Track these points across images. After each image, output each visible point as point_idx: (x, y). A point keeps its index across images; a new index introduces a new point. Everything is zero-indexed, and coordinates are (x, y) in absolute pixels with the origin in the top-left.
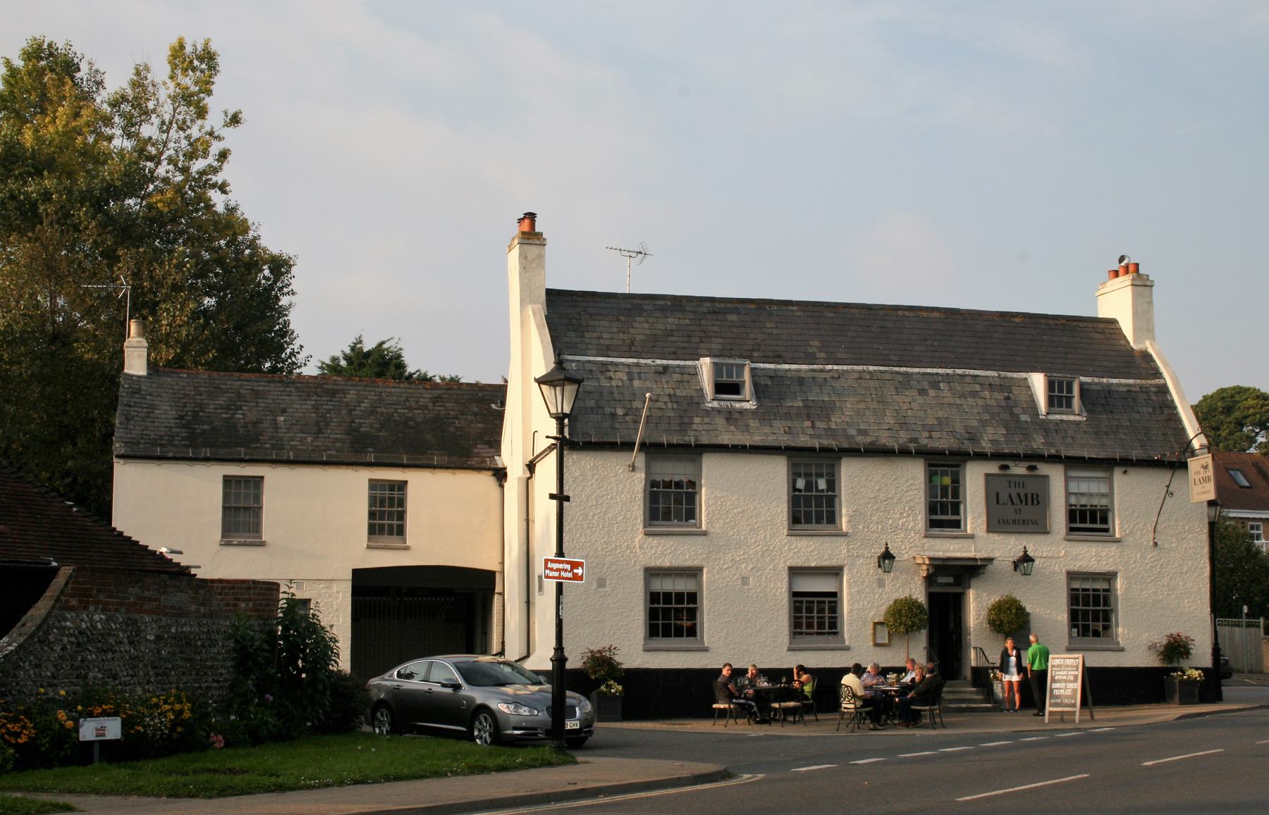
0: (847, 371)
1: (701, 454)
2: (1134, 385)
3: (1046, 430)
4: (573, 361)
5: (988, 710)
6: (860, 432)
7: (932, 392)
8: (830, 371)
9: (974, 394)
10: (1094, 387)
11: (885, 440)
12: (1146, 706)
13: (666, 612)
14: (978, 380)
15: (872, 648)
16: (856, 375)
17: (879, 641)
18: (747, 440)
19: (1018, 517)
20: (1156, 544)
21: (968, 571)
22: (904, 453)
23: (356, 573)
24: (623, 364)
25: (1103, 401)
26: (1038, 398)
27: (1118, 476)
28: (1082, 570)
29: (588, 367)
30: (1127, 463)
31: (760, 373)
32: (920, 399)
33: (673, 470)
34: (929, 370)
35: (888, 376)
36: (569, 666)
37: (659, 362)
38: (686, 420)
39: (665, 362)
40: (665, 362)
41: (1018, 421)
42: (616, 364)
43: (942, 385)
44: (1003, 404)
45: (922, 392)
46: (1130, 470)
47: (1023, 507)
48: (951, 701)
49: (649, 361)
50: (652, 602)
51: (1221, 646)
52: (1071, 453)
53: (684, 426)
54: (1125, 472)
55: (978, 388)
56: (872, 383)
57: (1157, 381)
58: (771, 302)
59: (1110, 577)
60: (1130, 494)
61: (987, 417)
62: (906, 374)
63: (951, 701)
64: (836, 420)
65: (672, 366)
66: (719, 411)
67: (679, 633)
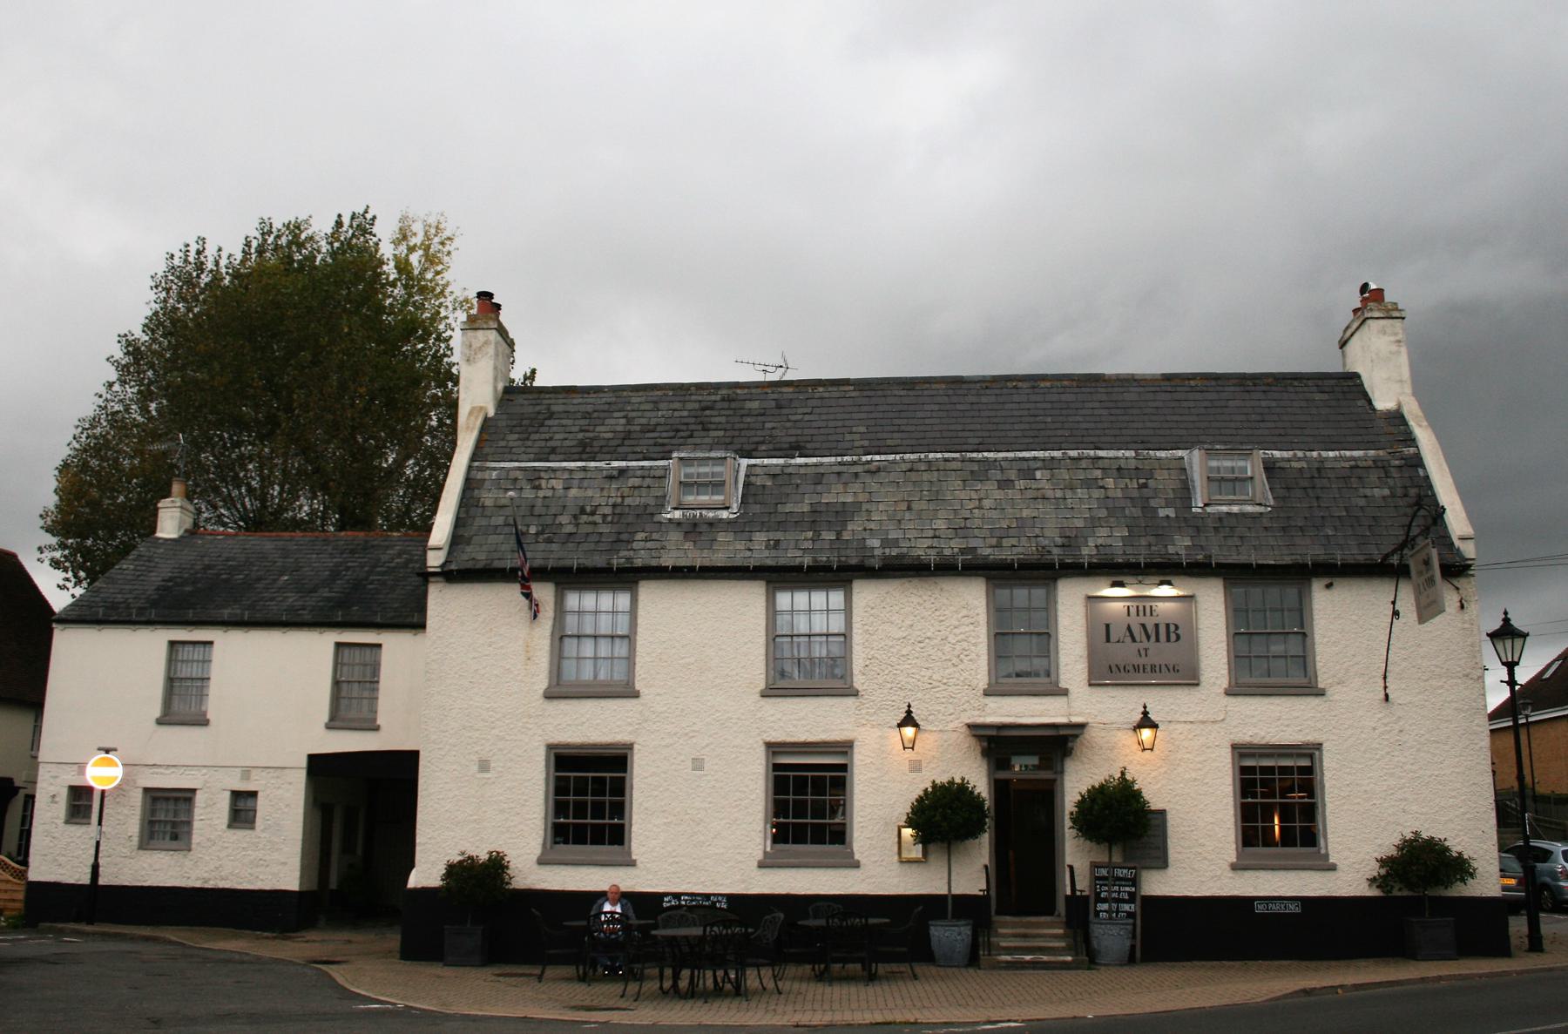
0: (894, 462)
1: (636, 583)
2: (1365, 459)
3: (1198, 529)
4: (494, 469)
5: (1065, 966)
6: (886, 543)
7: (1021, 484)
8: (868, 462)
9: (1089, 484)
10: (1295, 464)
11: (922, 549)
12: (1362, 963)
13: (598, 811)
14: (1101, 464)
15: (897, 865)
16: (904, 467)
17: (905, 855)
18: (719, 558)
19: (1141, 661)
20: (1387, 697)
21: (1058, 743)
22: (945, 569)
23: (313, 759)
24: (565, 469)
25: (1305, 484)
26: (1289, 486)
27: (866, 594)
28: (1256, 741)
29: (513, 475)
30: (1333, 571)
31: (758, 471)
32: (998, 494)
33: (813, 609)
34: (1040, 454)
35: (954, 465)
36: (101, 882)
37: (616, 464)
38: (624, 537)
39: (623, 464)
40: (623, 464)
41: (1155, 516)
42: (554, 470)
43: (1038, 474)
44: (1135, 494)
45: (1005, 484)
46: (1337, 581)
47: (1152, 644)
48: (1009, 950)
49: (602, 464)
50: (1244, 795)
51: (101, 861)
52: (1234, 558)
53: (620, 541)
54: (1329, 586)
55: (1098, 473)
56: (926, 476)
57: (1412, 450)
58: (1044, 377)
59: (845, 747)
60: (1344, 619)
61: (1103, 513)
62: (986, 460)
63: (1009, 950)
64: (854, 527)
65: (634, 469)
66: (679, 523)
67: (598, 840)
